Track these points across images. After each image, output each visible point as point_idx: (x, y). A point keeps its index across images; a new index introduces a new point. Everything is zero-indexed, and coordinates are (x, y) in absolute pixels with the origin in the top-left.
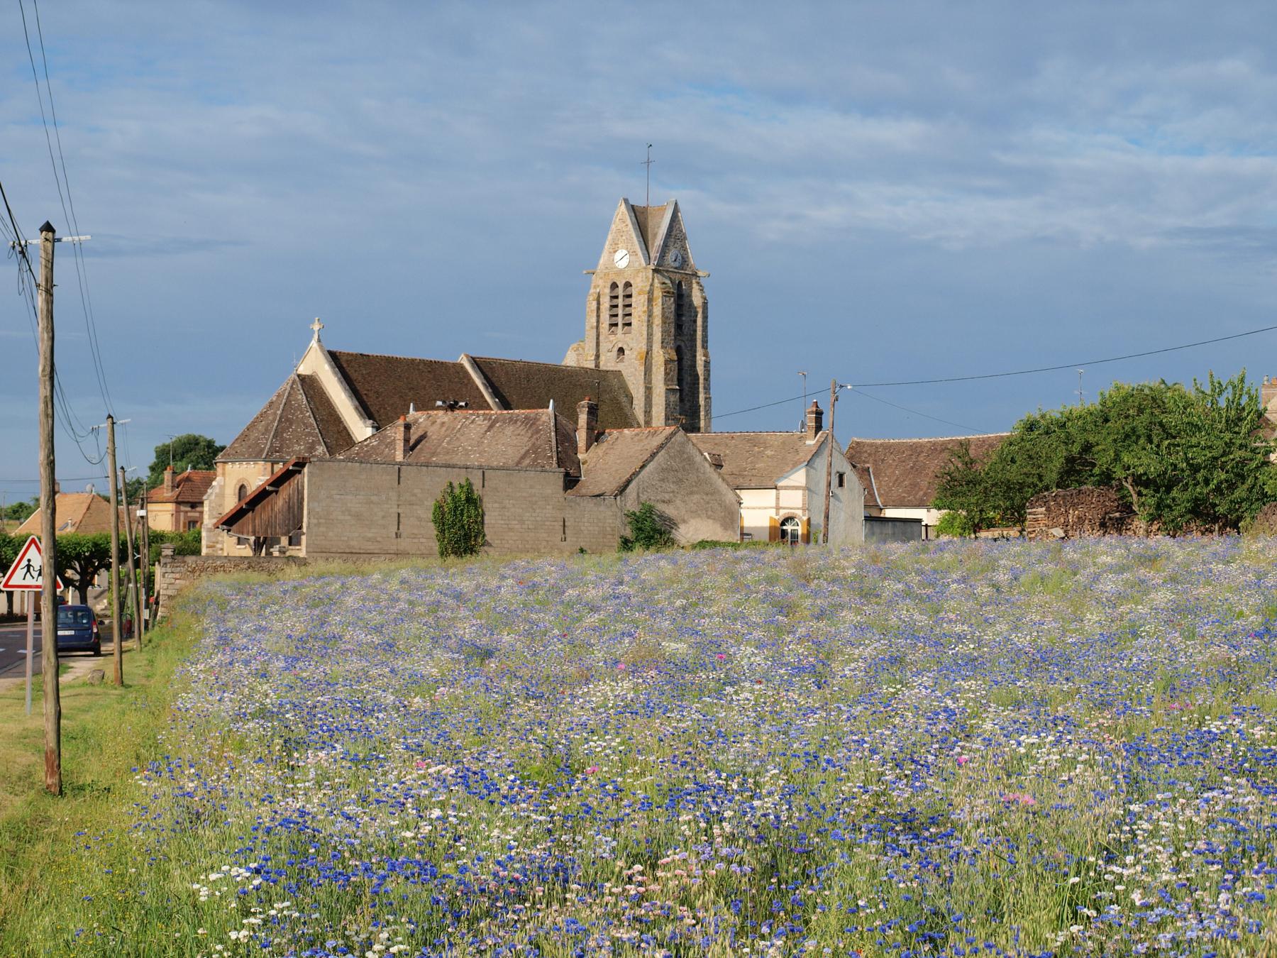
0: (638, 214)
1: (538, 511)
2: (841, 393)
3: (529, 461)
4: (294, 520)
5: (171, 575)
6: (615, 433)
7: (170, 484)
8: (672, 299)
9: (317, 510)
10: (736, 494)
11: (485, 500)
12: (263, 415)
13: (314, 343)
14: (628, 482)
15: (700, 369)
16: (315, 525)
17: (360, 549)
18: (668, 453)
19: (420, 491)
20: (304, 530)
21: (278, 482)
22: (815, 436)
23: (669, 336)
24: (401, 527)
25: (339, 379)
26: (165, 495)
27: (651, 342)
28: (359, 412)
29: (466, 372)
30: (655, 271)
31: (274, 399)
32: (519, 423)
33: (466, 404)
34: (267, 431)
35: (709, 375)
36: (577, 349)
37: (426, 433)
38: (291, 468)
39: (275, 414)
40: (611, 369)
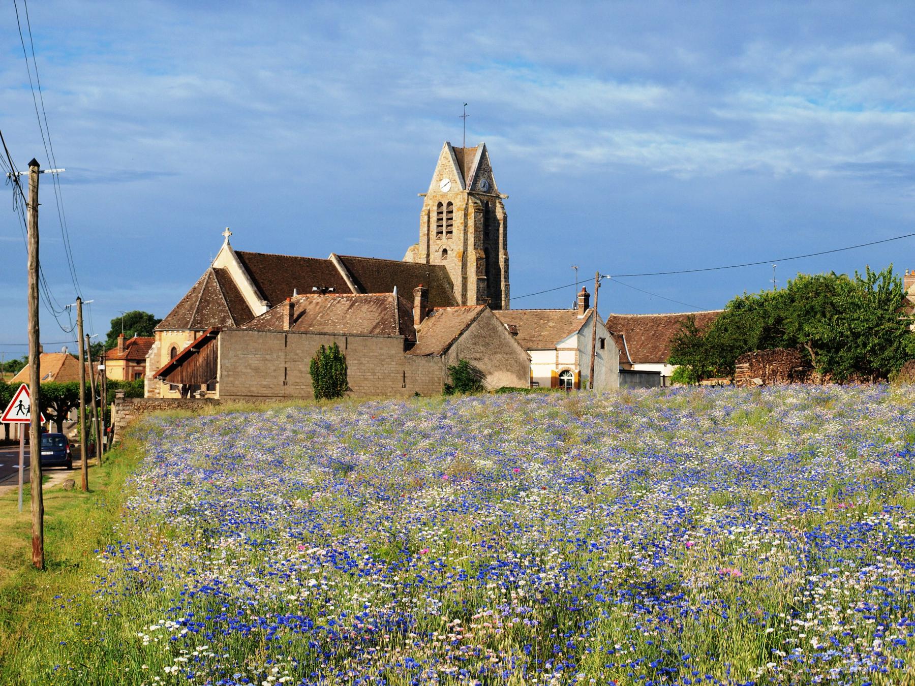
0: (457, 153)
1: (385, 366)
2: (602, 281)
3: (380, 329)
4: (210, 373)
5: (123, 412)
6: (441, 310)
7: (122, 346)
8: (482, 214)
9: (227, 365)
10: (528, 354)
11: (348, 358)
12: (188, 297)
13: (225, 246)
14: (450, 345)
15: (502, 264)
16: (226, 376)
17: (258, 393)
18: (479, 324)
19: (301, 352)
20: (218, 379)
21: (199, 345)
22: (584, 312)
23: (479, 241)
24: (287, 377)
25: (243, 271)
26: (119, 354)
27: (467, 245)
28: (258, 295)
29: (334, 267)
30: (469, 194)
31: (197, 286)
32: (372, 303)
33: (334, 289)
34: (191, 308)
35: (508, 269)
36: (414, 250)
37: (305, 310)
38: (208, 335)
39: (197, 296)
40: (438, 264)
